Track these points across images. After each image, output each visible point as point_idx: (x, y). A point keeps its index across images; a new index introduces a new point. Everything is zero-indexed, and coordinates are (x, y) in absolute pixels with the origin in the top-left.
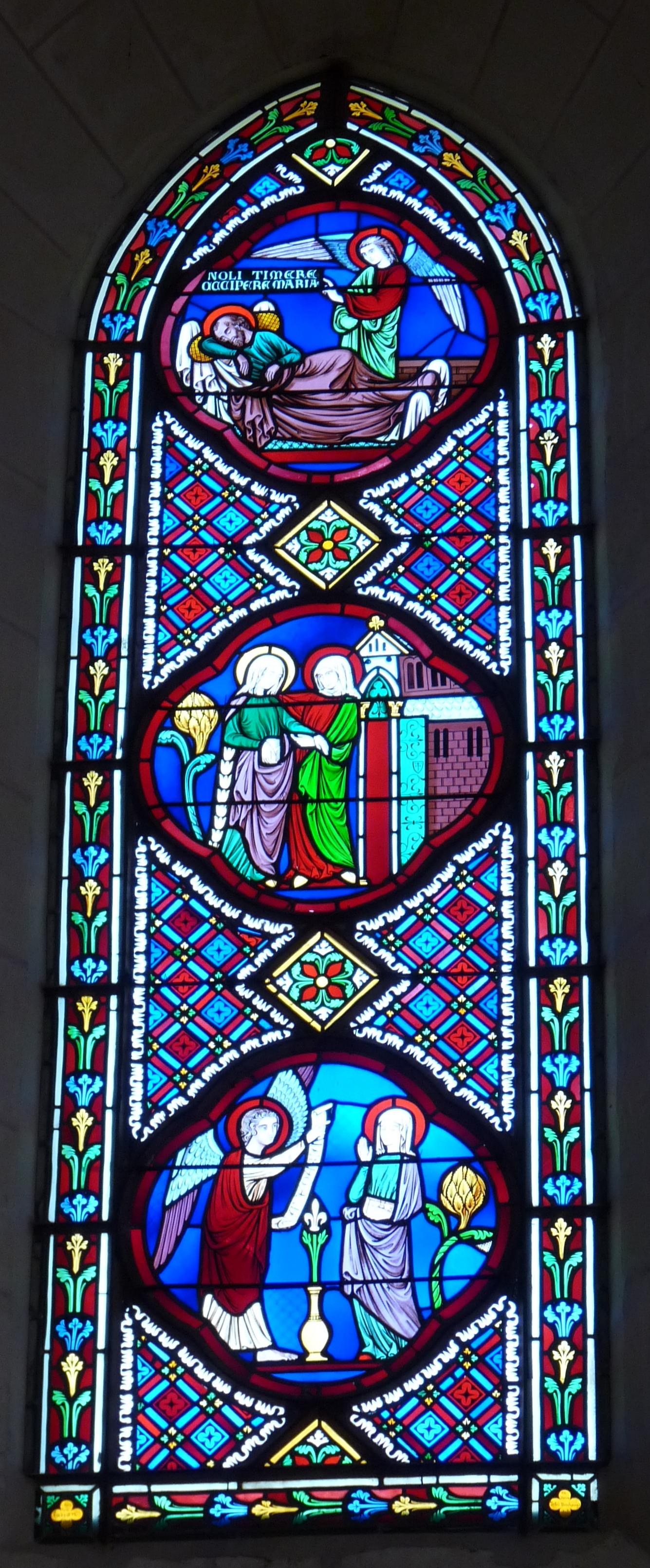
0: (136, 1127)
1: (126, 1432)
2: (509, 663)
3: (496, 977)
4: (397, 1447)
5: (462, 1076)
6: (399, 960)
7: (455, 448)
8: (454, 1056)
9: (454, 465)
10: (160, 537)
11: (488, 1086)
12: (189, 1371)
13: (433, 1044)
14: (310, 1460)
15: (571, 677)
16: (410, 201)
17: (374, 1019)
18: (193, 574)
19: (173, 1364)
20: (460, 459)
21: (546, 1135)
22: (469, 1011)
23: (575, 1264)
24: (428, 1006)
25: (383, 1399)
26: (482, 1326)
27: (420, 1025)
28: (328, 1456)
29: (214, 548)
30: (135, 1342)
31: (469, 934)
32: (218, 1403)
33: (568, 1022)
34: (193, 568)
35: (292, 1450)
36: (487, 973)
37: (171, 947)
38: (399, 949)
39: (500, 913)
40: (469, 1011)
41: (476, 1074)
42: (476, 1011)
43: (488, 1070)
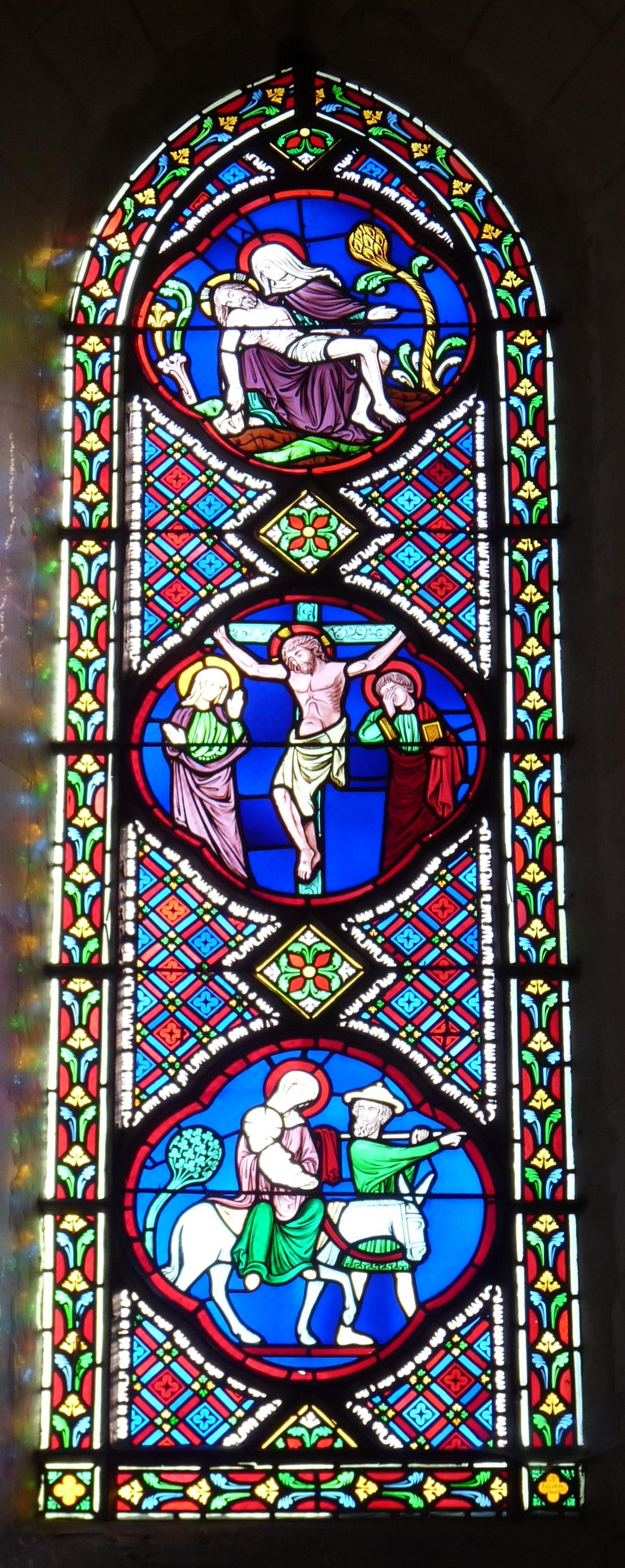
0: (127, 1115)
1: (122, 1410)
2: (489, 666)
3: (478, 978)
4: (381, 515)
5: (447, 1071)
6: (381, 515)
7: (435, 439)
8: (435, 489)
9: (433, 456)
10: (144, 522)
11: (466, 632)
12: (183, 1352)
13: (415, 593)
14: (303, 1443)
15: (551, 715)
16: (387, 191)
17: (360, 567)
18: (178, 501)
19: (168, 1346)
20: (440, 450)
21: (532, 1299)
22: (452, 1008)
23: (555, 1121)
24: (409, 556)
25: (372, 586)
26: (455, 418)
27: (405, 575)
28: (321, 1438)
29: (196, 533)
30: (137, 853)
31: (448, 551)
32: (211, 1385)
33: (541, 782)
34: (177, 495)
35: (285, 1432)
36: (462, 530)
37: (164, 502)
38: (383, 505)
39: (477, 591)
40: (452, 1008)
41: (461, 1069)
42: (458, 1008)
43: (473, 1065)
